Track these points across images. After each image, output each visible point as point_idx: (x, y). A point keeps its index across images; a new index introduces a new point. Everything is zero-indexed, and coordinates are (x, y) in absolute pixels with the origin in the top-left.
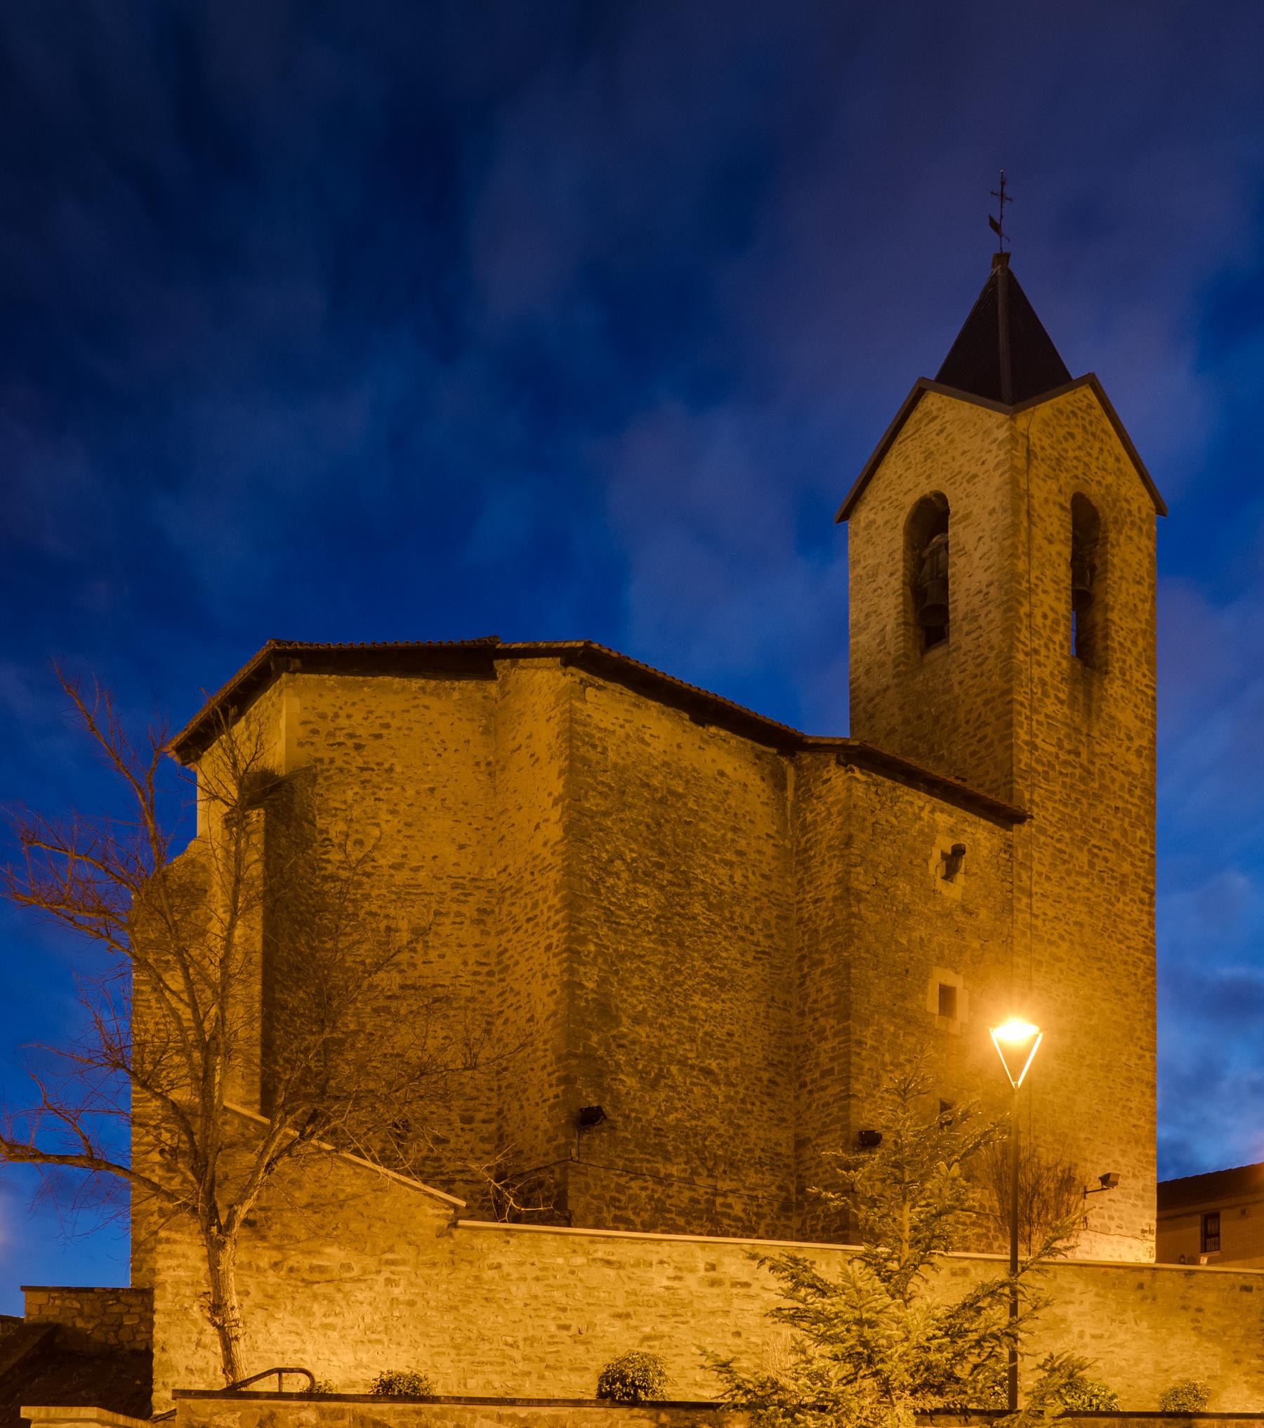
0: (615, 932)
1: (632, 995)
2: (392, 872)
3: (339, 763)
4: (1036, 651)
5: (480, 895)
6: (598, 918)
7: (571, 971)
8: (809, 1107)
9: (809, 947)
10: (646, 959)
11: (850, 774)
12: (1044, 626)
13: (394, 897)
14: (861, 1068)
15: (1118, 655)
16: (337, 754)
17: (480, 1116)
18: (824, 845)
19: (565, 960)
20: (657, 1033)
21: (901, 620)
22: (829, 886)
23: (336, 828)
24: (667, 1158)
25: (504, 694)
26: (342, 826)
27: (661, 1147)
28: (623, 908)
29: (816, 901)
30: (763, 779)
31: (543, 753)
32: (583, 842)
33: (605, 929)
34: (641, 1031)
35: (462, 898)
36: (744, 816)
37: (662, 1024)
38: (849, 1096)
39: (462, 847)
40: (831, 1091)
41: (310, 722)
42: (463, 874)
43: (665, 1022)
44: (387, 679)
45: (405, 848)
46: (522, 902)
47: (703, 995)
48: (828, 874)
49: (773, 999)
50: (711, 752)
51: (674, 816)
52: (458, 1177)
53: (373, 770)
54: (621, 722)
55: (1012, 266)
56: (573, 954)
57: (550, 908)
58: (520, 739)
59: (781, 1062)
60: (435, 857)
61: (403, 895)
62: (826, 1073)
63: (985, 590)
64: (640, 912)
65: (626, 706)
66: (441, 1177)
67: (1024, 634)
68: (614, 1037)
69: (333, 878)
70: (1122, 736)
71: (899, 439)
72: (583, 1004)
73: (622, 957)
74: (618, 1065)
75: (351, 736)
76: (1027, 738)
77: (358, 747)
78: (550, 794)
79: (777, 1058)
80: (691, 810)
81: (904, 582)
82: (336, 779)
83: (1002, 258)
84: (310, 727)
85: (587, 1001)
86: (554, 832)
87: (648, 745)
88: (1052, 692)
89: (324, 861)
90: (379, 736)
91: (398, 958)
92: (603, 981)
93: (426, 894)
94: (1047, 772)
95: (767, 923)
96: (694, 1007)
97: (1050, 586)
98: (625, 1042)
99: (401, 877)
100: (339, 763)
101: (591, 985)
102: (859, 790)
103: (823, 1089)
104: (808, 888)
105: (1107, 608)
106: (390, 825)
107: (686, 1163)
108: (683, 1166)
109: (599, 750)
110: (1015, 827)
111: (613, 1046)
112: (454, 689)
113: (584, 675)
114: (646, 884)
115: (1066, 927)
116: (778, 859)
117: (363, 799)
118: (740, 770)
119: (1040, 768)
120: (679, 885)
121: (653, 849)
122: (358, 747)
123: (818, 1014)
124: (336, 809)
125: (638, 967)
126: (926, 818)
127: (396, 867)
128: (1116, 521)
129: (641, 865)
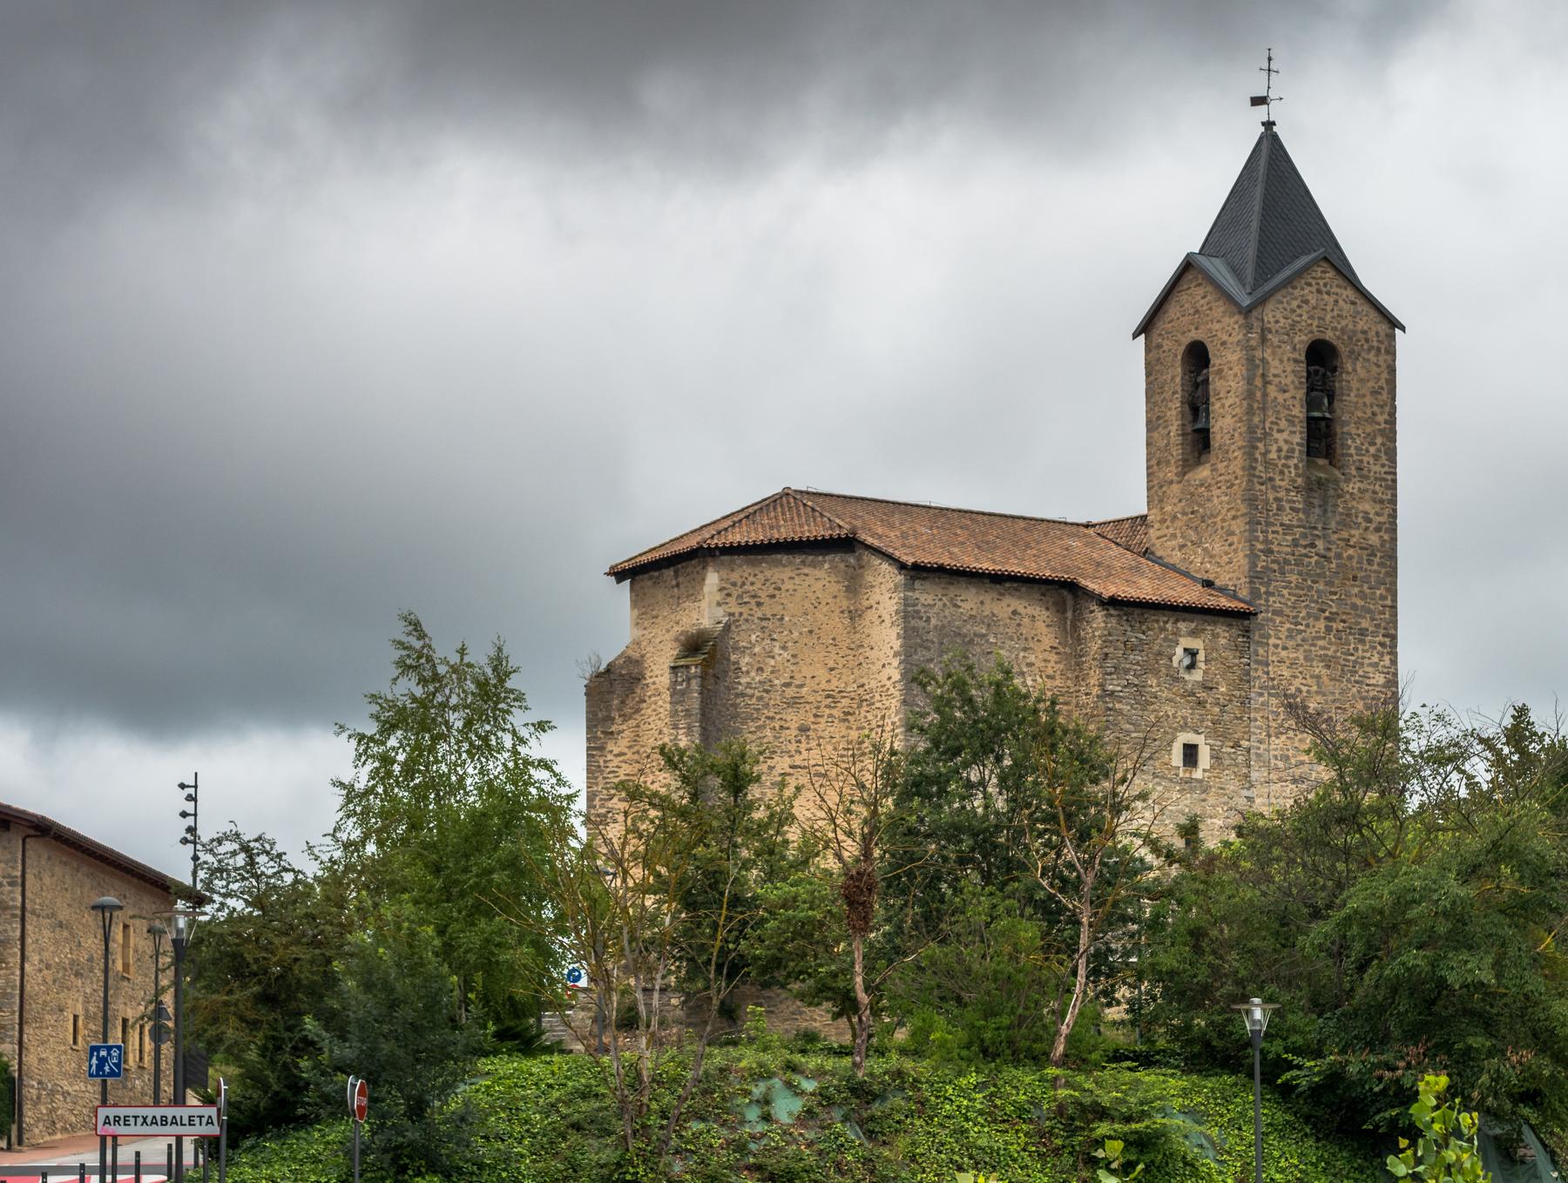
4: (1271, 479)
5: (845, 702)
16: (744, 609)
26: (747, 659)
50: (1007, 600)
58: (872, 602)
69: (743, 695)
75: (754, 597)
77: (759, 604)
83: (1269, 125)
88: (1287, 506)
90: (773, 596)
97: (1283, 424)
99: (790, 692)
106: (782, 656)
119: (1275, 566)
127: (787, 685)
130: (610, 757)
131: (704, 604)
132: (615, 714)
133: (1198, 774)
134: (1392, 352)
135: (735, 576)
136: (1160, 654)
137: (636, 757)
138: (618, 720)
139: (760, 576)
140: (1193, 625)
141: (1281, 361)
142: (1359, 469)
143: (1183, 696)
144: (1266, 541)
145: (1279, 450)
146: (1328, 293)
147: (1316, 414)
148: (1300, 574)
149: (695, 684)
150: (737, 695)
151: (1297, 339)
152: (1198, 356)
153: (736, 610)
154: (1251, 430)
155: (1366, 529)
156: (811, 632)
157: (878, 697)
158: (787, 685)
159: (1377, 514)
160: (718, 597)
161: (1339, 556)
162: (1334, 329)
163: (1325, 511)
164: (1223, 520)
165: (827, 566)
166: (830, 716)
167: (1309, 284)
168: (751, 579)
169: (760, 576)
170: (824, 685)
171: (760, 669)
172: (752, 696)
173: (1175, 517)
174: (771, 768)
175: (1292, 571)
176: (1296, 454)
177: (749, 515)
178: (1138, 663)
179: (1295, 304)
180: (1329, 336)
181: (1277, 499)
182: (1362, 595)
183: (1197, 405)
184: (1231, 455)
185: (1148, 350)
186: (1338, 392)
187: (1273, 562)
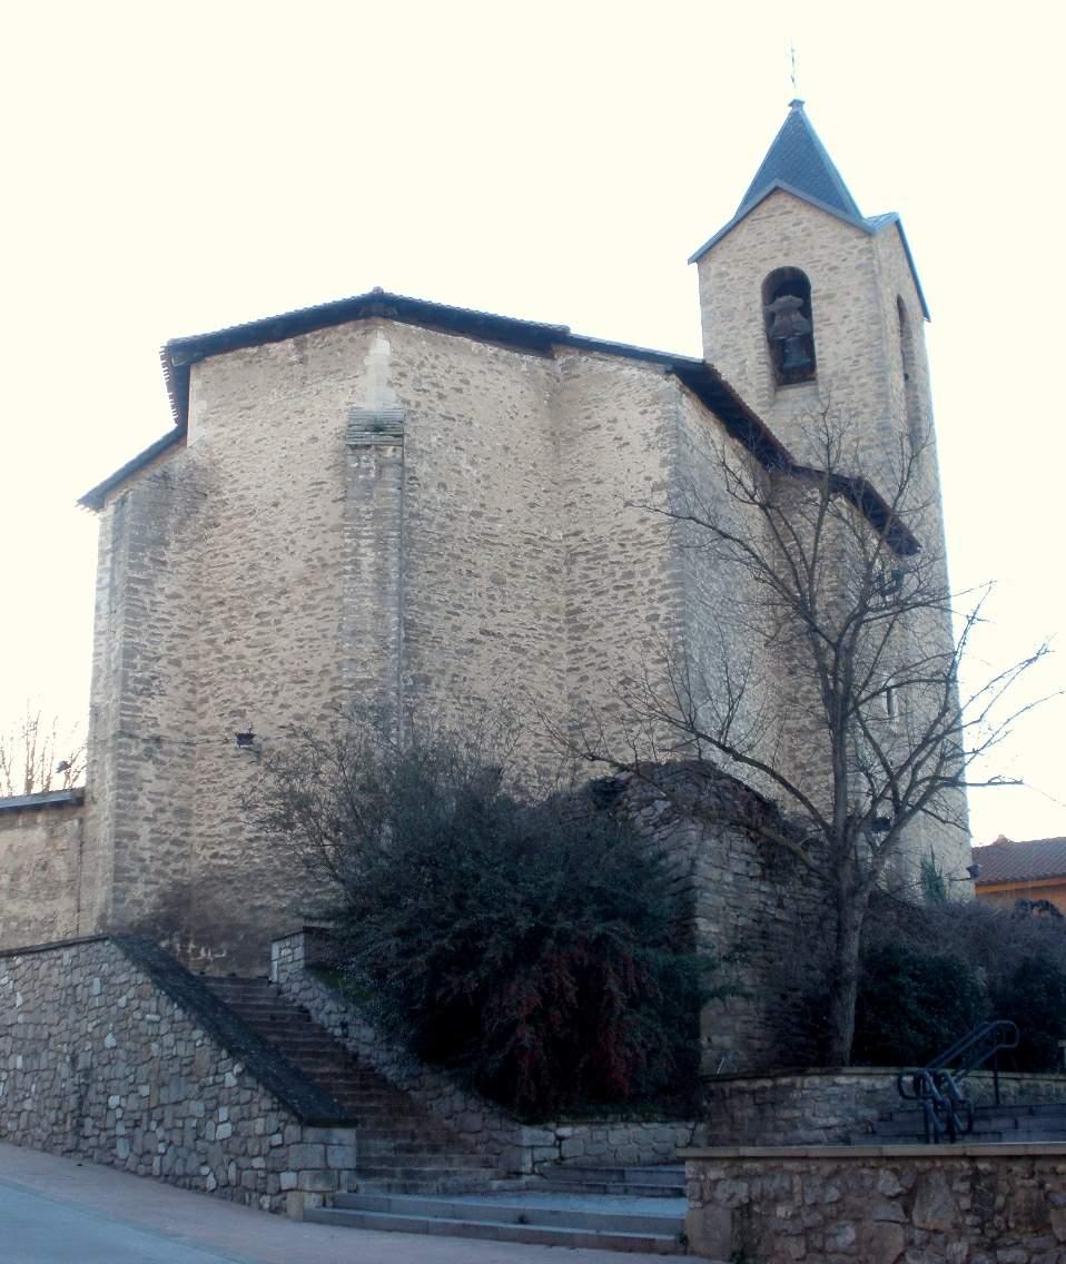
77: (441, 397)
127: (477, 514)
130: (160, 598)
132: (171, 537)
137: (195, 604)
138: (174, 546)
153: (412, 397)
158: (477, 514)
165: (524, 368)
166: (531, 568)
170: (522, 526)
172: (431, 521)
174: (456, 628)
177: (741, 208)
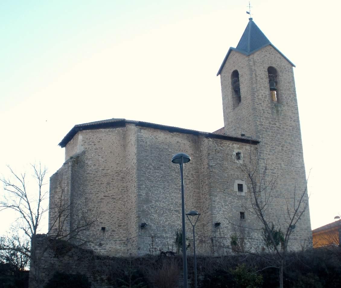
0: (150, 181)
1: (155, 195)
2: (102, 171)
3: (90, 148)
4: (260, 103)
6: (145, 179)
7: (139, 192)
8: (205, 217)
9: (203, 179)
10: (159, 187)
11: (208, 140)
12: (262, 97)
13: (103, 176)
14: (215, 207)
15: (285, 100)
16: (90, 146)
17: (123, 225)
18: (204, 156)
19: (137, 190)
20: (162, 203)
21: (232, 97)
22: (206, 165)
23: (90, 163)
24: (166, 233)
25: (127, 130)
27: (164, 230)
28: (152, 176)
29: (204, 168)
30: (189, 142)
31: (133, 144)
32: (141, 163)
33: (147, 182)
34: (158, 204)
35: (118, 175)
36: (185, 151)
37: (163, 201)
38: (212, 214)
39: (118, 164)
40: (209, 213)
41: (84, 140)
42: (118, 170)
43: (164, 201)
44: (101, 129)
45: (105, 165)
46: (130, 176)
47: (175, 193)
48: (206, 162)
49: (195, 192)
50: (175, 138)
51: (165, 154)
52: (117, 239)
53: (98, 149)
54: (151, 135)
55: (253, 20)
56: (139, 188)
57: (135, 178)
59: (198, 206)
60: (112, 167)
61: (106, 175)
62: (208, 209)
63: (247, 91)
64: (157, 176)
65: (152, 132)
66: (114, 240)
67: (257, 100)
68: (150, 206)
69: (88, 173)
70: (289, 118)
71: (228, 59)
72: (142, 199)
73: (152, 187)
74: (152, 212)
75: (93, 142)
76: (259, 123)
78: (134, 153)
79: (197, 205)
80: (170, 151)
81: (232, 89)
82: (90, 152)
83: (251, 19)
84: (84, 141)
85: (143, 198)
86: (135, 161)
87: (158, 139)
88: (266, 112)
89: (87, 170)
90: (99, 142)
91: (54, 212)
92: (147, 194)
93: (109, 175)
94: (266, 130)
95: (192, 174)
96: (172, 196)
97: (263, 88)
98: (153, 206)
99: (104, 172)
100: (90, 148)
101: (144, 195)
102: (211, 143)
103: (207, 212)
104: (202, 165)
105: (281, 90)
107: (171, 233)
108: (171, 234)
109: (145, 142)
110: (258, 144)
111: (150, 208)
112: (116, 130)
113: (140, 127)
114: (158, 170)
115: (276, 165)
116: (195, 159)
117: (96, 155)
118: (183, 141)
119: (264, 129)
120: (167, 169)
121: (160, 162)
122: (95, 145)
123: (205, 195)
124: (90, 158)
125: (157, 189)
126: (231, 146)
127: (103, 170)
128: (281, 71)
129: (157, 166)
131: (78, 146)
133: (243, 194)
134: (292, 72)
135: (87, 136)
136: (227, 154)
139: (95, 136)
140: (238, 146)
141: (260, 71)
142: (287, 103)
143: (236, 168)
144: (260, 122)
145: (262, 95)
146: (272, 54)
147: (272, 87)
148: (272, 132)
149: (70, 168)
150: (88, 174)
151: (264, 65)
152: (235, 74)
153: (87, 147)
154: (253, 89)
155: (291, 121)
156: (111, 152)
157: (131, 170)
158: (103, 170)
159: (294, 117)
160: (82, 143)
161: (283, 128)
162: (275, 64)
163: (278, 115)
164: (247, 118)
166: (117, 179)
167: (267, 51)
168: (92, 137)
169: (95, 136)
170: (115, 169)
171: (95, 165)
172: (91, 174)
173: (232, 122)
175: (269, 131)
176: (268, 97)
178: (220, 157)
179: (263, 56)
180: (274, 66)
181: (263, 110)
182: (292, 140)
183: (236, 90)
184: (247, 98)
185: (221, 78)
186: (278, 82)
187: (263, 128)
